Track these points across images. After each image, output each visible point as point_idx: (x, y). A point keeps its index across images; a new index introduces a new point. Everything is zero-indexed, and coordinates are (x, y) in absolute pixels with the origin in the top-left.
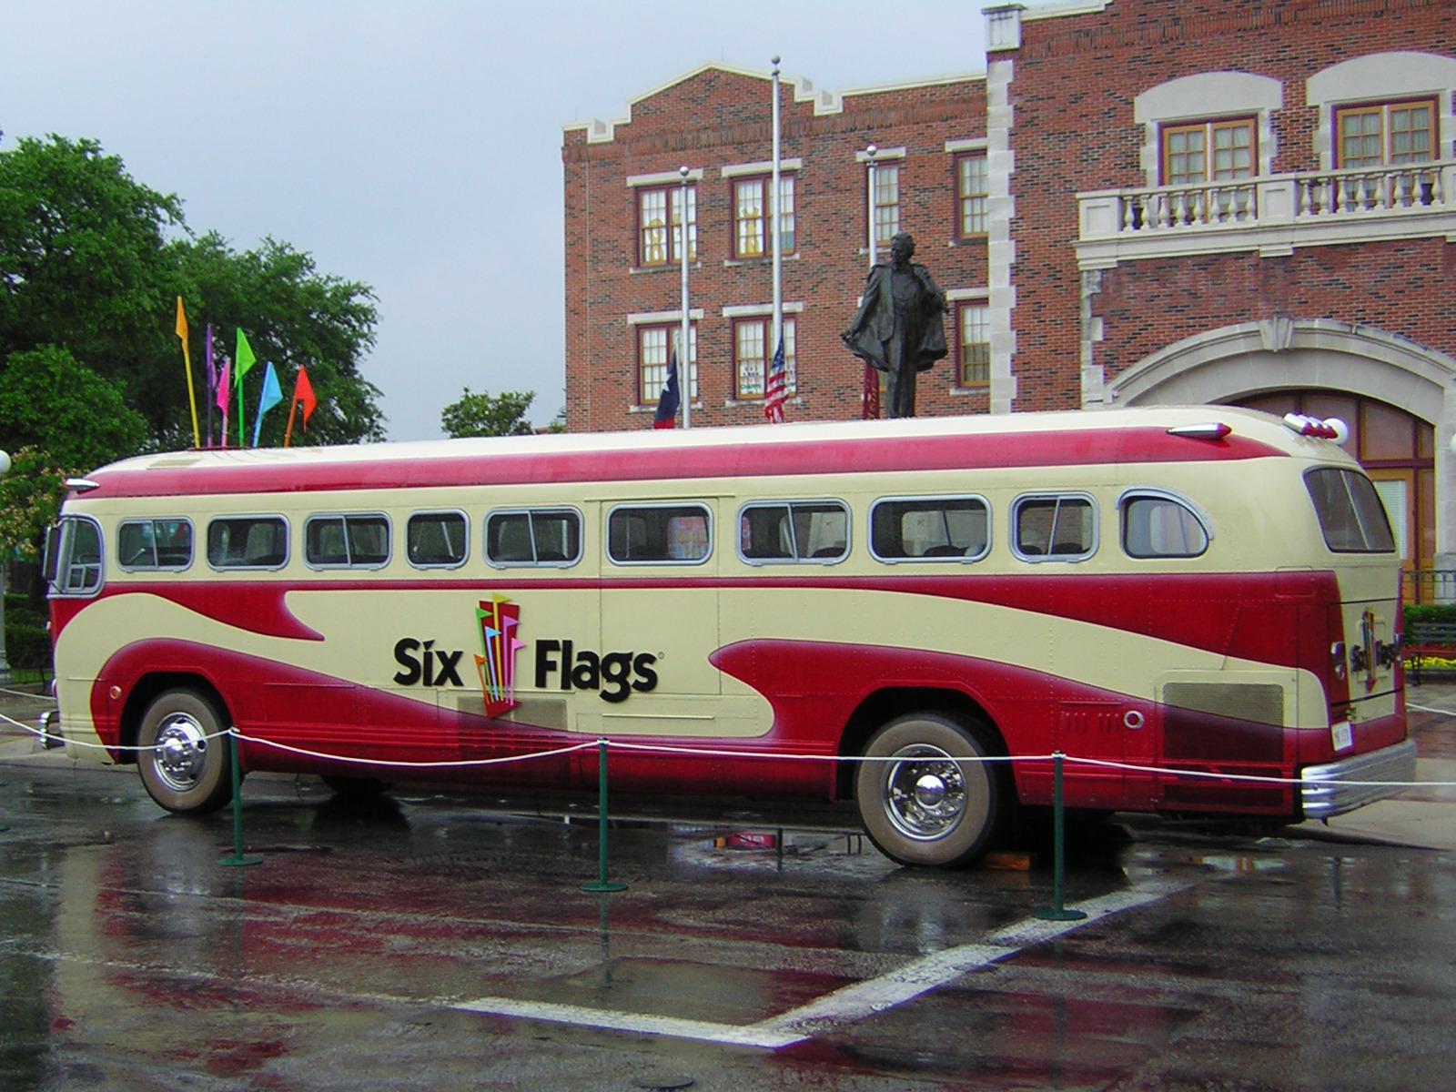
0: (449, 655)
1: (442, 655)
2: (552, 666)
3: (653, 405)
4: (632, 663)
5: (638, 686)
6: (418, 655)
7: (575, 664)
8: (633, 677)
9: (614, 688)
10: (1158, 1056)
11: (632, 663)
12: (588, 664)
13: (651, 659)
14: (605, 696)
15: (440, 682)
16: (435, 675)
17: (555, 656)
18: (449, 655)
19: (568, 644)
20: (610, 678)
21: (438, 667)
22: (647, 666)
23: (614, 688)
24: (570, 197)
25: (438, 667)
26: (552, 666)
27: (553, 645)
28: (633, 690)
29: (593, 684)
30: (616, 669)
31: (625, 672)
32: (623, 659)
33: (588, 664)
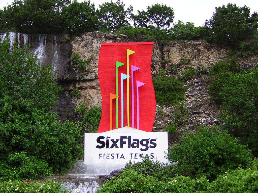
0: (115, 141)
1: (113, 141)
2: (125, 143)
3: (22, 38)
4: (149, 141)
5: (151, 147)
6: (105, 140)
7: (132, 142)
8: (149, 145)
9: (144, 147)
10: (245, 165)
11: (149, 141)
12: (136, 142)
13: (155, 140)
14: (141, 150)
15: (112, 147)
16: (110, 146)
17: (126, 140)
18: (115, 141)
19: (130, 137)
20: (143, 145)
21: (111, 143)
22: (153, 142)
23: (144, 147)
24: (114, 81)
25: (111, 143)
26: (125, 143)
27: (126, 137)
28: (149, 148)
29: (138, 147)
30: (144, 143)
31: (147, 143)
32: (147, 140)
33: (136, 142)
